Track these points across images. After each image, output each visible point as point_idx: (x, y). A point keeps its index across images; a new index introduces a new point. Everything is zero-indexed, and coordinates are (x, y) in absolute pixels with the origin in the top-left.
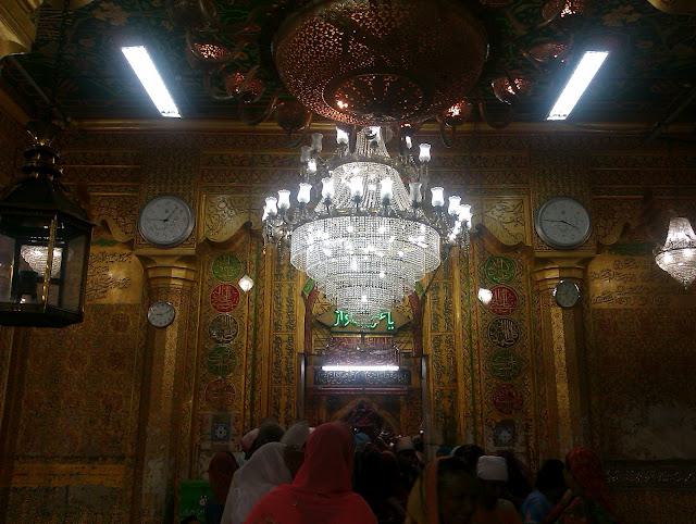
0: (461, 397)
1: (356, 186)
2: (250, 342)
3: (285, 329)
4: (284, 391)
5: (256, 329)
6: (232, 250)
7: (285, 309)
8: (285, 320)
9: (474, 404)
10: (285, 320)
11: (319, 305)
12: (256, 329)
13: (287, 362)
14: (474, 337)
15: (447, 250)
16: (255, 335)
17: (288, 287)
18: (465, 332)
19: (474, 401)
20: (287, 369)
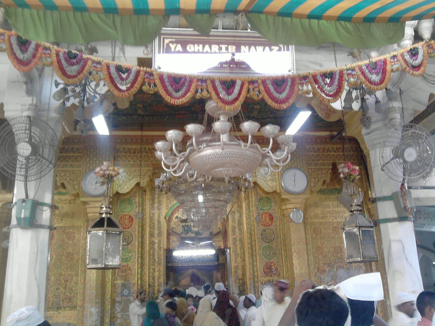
4: (156, 269)
13: (158, 254)
20: (158, 258)
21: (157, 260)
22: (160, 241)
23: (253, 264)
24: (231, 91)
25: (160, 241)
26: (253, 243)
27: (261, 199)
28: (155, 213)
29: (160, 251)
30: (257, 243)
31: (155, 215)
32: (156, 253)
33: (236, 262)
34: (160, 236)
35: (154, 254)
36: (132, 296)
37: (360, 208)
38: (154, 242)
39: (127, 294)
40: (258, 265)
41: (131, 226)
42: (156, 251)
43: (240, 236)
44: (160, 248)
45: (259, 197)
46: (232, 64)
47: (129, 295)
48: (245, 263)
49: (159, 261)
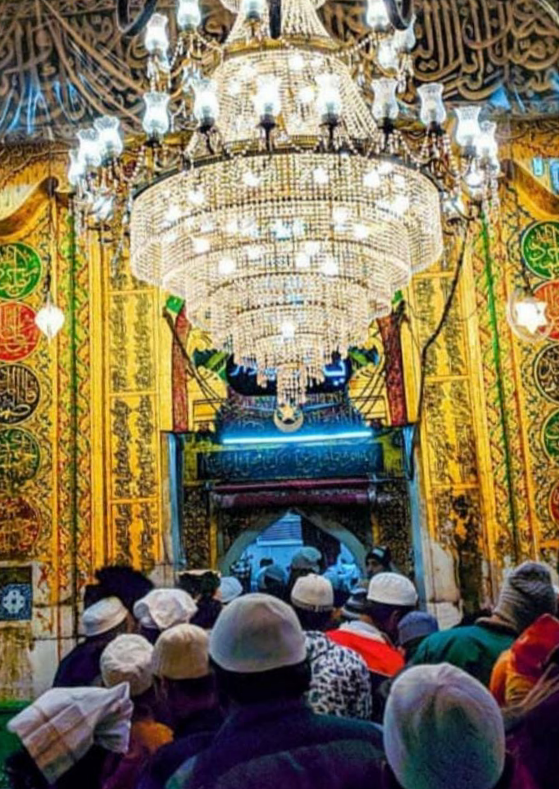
0: (485, 463)
1: (268, 96)
2: (64, 379)
3: (133, 385)
4: (136, 509)
5: (75, 390)
6: (22, 233)
7: (131, 345)
8: (131, 368)
9: (513, 517)
10: (131, 368)
11: (197, 333)
12: (75, 390)
13: (141, 450)
14: (508, 385)
15: (458, 386)
16: (74, 399)
17: (136, 302)
18: (496, 453)
19: (509, 472)
20: (142, 465)
21: (137, 472)
22: (146, 403)
23: (510, 485)
24: (476, 580)
25: (146, 403)
26: (511, 405)
27: (533, 232)
28: (126, 299)
29: (149, 442)
30: (523, 403)
31: (125, 305)
32: (133, 448)
33: (442, 477)
34: (147, 384)
35: (126, 450)
36: (39, 616)
37: (84, 19)
38: (123, 405)
39: (19, 605)
40: (532, 493)
41: (31, 348)
42: (133, 439)
43: (456, 377)
44: (147, 430)
45: (525, 222)
46: (466, 550)
47: (26, 613)
48: (478, 481)
49: (143, 477)
